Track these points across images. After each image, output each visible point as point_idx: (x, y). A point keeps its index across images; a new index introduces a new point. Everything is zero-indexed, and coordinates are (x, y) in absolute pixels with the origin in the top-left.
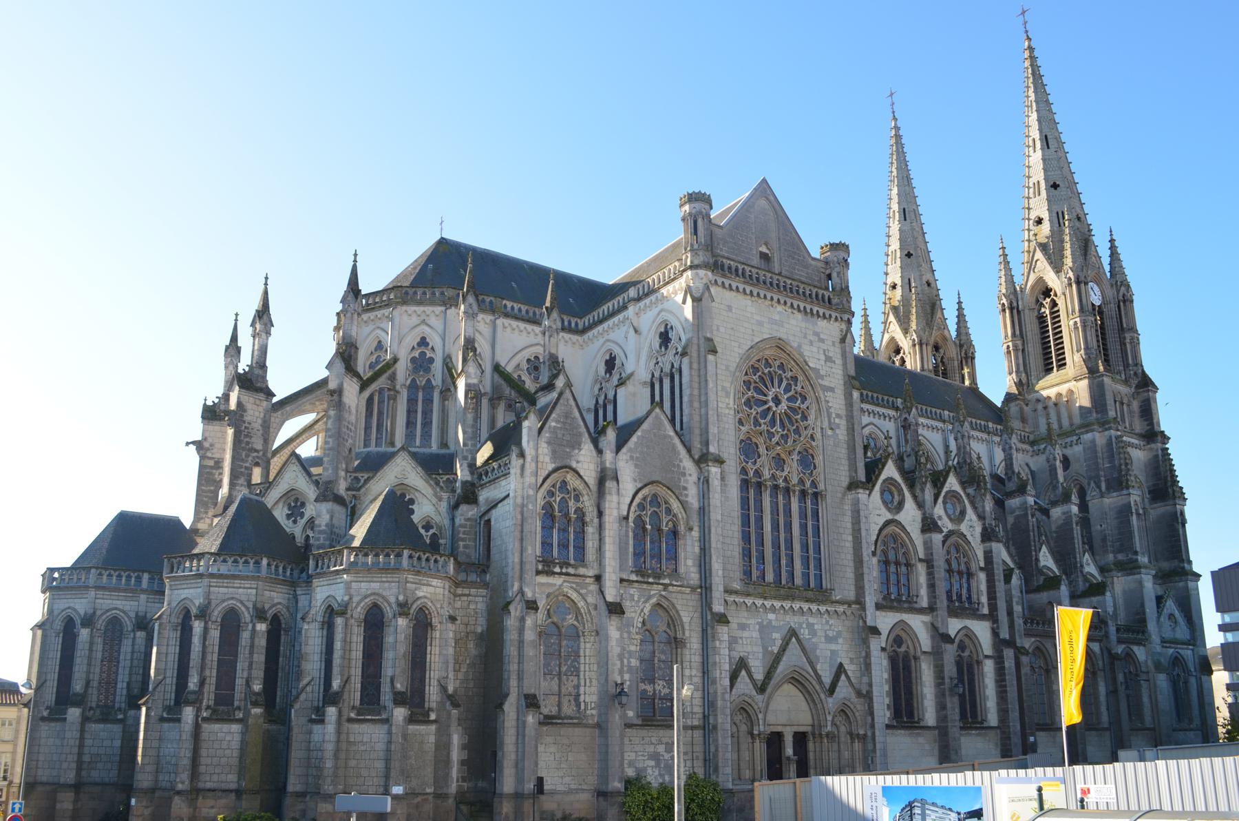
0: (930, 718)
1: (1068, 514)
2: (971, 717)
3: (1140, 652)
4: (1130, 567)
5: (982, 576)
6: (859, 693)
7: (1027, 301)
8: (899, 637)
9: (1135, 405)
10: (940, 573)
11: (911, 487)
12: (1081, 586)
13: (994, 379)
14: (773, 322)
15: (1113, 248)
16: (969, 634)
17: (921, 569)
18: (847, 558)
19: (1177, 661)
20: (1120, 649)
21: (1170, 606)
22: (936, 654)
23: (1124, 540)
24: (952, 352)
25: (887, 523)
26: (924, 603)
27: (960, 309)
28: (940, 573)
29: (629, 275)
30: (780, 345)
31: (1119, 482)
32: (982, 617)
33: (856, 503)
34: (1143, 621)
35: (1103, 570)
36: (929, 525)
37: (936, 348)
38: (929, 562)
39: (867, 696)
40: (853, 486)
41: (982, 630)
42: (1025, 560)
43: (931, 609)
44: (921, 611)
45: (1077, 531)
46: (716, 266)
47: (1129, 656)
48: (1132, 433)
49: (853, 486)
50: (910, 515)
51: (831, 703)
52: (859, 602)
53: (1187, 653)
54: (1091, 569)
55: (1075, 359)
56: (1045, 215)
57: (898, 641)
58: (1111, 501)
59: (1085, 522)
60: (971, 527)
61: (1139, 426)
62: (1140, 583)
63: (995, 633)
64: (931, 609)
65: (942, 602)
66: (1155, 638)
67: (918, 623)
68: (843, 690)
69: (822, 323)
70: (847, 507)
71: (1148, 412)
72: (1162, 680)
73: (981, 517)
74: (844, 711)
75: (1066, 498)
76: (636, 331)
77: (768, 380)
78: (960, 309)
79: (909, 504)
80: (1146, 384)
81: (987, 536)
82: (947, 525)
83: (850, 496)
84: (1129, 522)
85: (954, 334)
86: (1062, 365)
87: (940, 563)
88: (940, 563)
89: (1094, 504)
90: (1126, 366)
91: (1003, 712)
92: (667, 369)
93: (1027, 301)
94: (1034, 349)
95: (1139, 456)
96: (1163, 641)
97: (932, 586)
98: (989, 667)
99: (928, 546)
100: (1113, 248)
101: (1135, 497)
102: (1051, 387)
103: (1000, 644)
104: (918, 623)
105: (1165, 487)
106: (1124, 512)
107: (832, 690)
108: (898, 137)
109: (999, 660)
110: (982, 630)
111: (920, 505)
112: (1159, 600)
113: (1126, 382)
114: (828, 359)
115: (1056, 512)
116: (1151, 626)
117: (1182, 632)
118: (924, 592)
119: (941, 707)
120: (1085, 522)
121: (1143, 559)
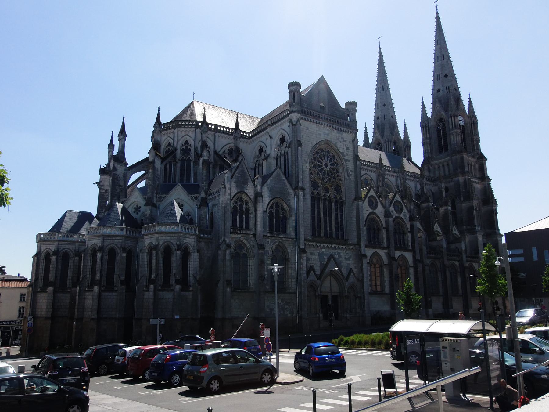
1: (446, 210)
5: (409, 235)
6: (358, 280)
9: (477, 166)
15: (470, 102)
20: (467, 264)
22: (390, 265)
25: (370, 214)
27: (405, 127)
28: (392, 233)
30: (328, 143)
31: (469, 197)
32: (409, 251)
33: (358, 206)
36: (387, 214)
38: (387, 229)
39: (362, 282)
41: (409, 256)
43: (388, 247)
44: (384, 248)
45: (450, 217)
48: (475, 177)
50: (380, 210)
52: (359, 244)
59: (454, 214)
60: (405, 215)
62: (477, 238)
63: (414, 257)
64: (388, 247)
67: (382, 253)
68: (352, 279)
69: (345, 134)
70: (354, 207)
71: (482, 168)
73: (409, 211)
76: (271, 137)
78: (405, 127)
80: (482, 159)
85: (402, 137)
90: (474, 150)
92: (283, 152)
93: (432, 123)
95: (478, 186)
97: (388, 239)
99: (387, 222)
100: (470, 102)
101: (475, 203)
104: (382, 253)
107: (347, 280)
110: (409, 256)
113: (473, 157)
114: (347, 148)
115: (442, 210)
118: (385, 241)
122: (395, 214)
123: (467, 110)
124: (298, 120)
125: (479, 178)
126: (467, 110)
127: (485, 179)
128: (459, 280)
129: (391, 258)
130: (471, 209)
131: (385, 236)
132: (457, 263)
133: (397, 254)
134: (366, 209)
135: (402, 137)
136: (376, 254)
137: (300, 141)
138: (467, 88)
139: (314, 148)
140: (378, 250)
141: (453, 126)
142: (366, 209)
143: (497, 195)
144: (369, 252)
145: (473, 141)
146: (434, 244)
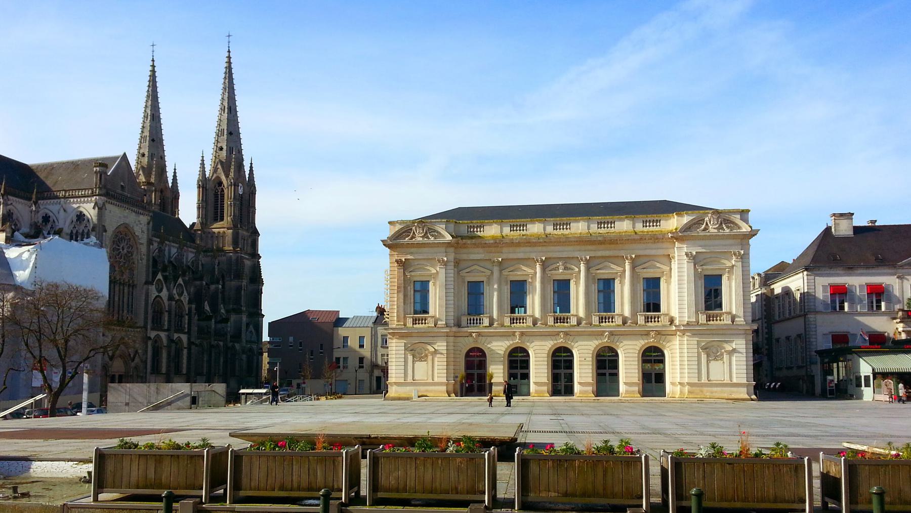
0: (164, 370)
1: (217, 289)
2: (178, 372)
3: (237, 346)
4: (238, 311)
5: (187, 317)
6: (142, 361)
7: (210, 186)
8: (157, 339)
9: (250, 241)
10: (173, 316)
11: (166, 282)
12: (219, 318)
13: (188, 211)
14: (125, 217)
15: (251, 167)
16: (180, 339)
17: (166, 314)
18: (142, 311)
19: (251, 350)
20: (230, 345)
21: (251, 328)
22: (169, 347)
23: (238, 301)
24: (169, 195)
25: (157, 297)
26: (166, 328)
27: (175, 173)
28: (173, 316)
29: (35, 165)
30: (126, 226)
31: (238, 276)
32: (185, 333)
33: (148, 289)
34: (240, 333)
35: (228, 311)
36: (171, 298)
37: (162, 191)
38: (169, 312)
39: (146, 362)
40: (147, 283)
41: (184, 338)
42: (200, 310)
43: (168, 330)
44: (164, 331)
45: (220, 295)
46: (107, 195)
47: (233, 347)
48: (246, 253)
49: (147, 283)
50: (164, 294)
51: (133, 364)
52: (145, 327)
53: (255, 346)
54: (223, 311)
55: (228, 219)
56: (225, 148)
57: (156, 342)
58: (234, 283)
59: (223, 293)
60: (185, 298)
61: (249, 250)
62: (241, 318)
63: (189, 339)
64: (168, 330)
65: (173, 329)
66: (244, 341)
67: (163, 335)
68: (137, 360)
69: (141, 216)
70: (144, 291)
71: (254, 244)
72: (244, 357)
73: (189, 294)
74: (136, 368)
75: (218, 283)
76: (65, 211)
77: (120, 240)
78: (175, 173)
79: (165, 290)
80: (256, 233)
81: (190, 302)
82: (177, 297)
83: (145, 287)
84: (240, 293)
85: (170, 185)
86: (222, 219)
87: (173, 313)
88: (173, 313)
89: (227, 283)
90: (249, 223)
91: (189, 368)
92: (81, 231)
93: (210, 186)
94: (211, 209)
95: (248, 263)
96: (247, 341)
97: (169, 321)
98: (185, 352)
99: (170, 306)
100: (251, 167)
101: (244, 283)
102: (218, 228)
103: (190, 343)
104: (163, 335)
105: (256, 279)
106: (239, 289)
107: (133, 360)
108: (153, 71)
109: (189, 349)
110: (184, 338)
111: (168, 290)
112: (248, 325)
113: (247, 230)
114: (143, 232)
115: (213, 287)
116: (243, 336)
117: (254, 338)
118: (166, 323)
119: (168, 366)
120: (223, 293)
121: (244, 309)
122: (177, 297)
123: (247, 176)
124: (104, 204)
125: (249, 254)
126: (247, 176)
127: (256, 256)
128: (222, 360)
129: (171, 340)
130: (239, 289)
131: (166, 319)
132: (221, 343)
133: (176, 336)
134: (154, 293)
135: (170, 185)
136: (158, 336)
137: (104, 226)
138: (251, 151)
139: (114, 232)
140: (159, 333)
141: (231, 190)
142: (154, 293)
143: (265, 275)
144: (153, 334)
145: (249, 213)
146: (684, 503)
